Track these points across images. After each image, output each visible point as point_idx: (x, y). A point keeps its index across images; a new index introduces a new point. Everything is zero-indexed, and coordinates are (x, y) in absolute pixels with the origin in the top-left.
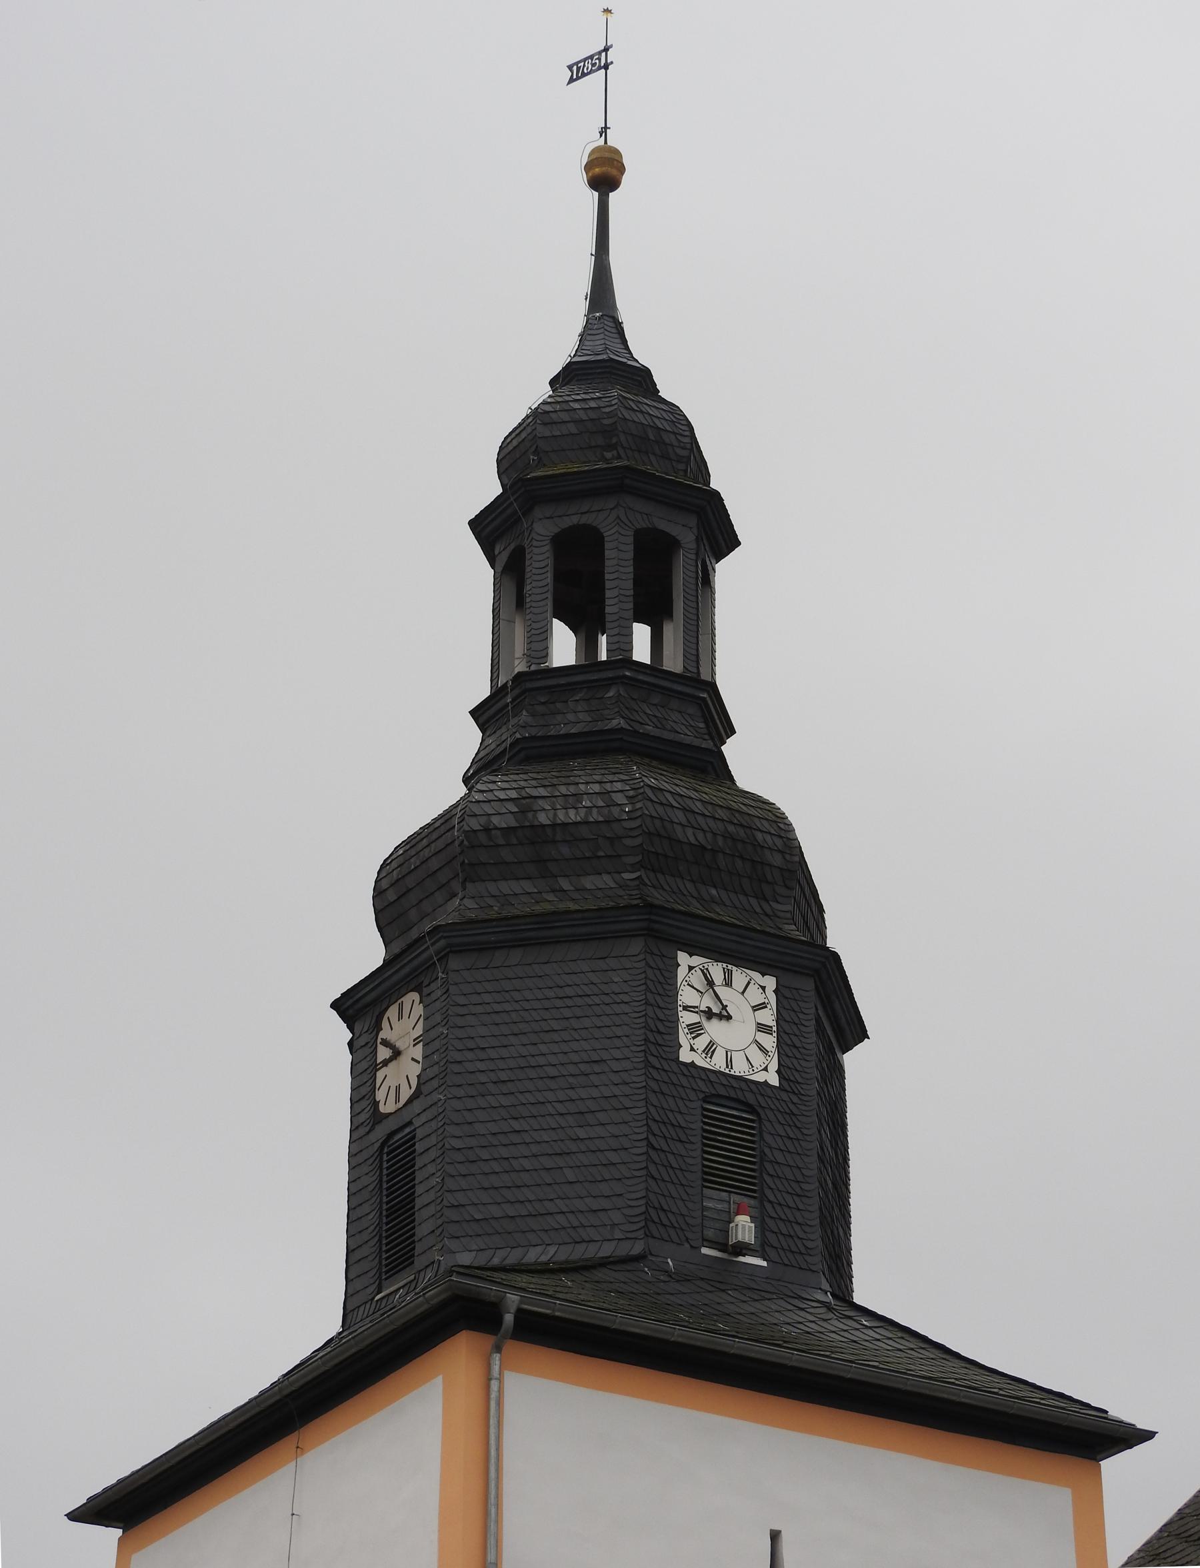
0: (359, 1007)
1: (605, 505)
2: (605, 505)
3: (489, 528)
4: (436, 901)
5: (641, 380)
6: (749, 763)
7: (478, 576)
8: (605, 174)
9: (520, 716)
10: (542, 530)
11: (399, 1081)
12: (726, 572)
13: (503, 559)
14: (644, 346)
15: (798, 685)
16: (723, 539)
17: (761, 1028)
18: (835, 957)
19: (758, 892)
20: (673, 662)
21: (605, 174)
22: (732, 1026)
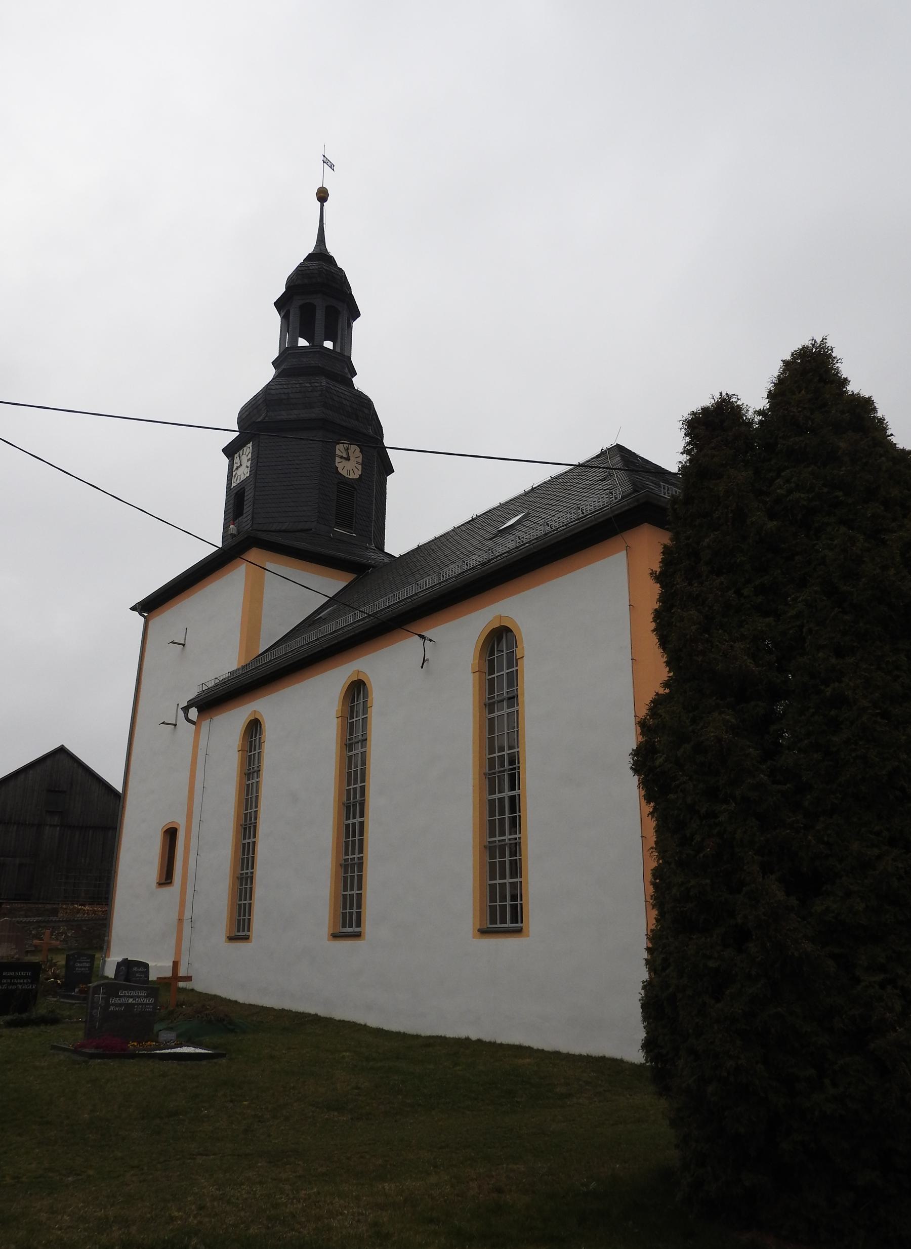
0: (230, 451)
1: (318, 298)
2: (318, 298)
3: (280, 304)
4: (260, 424)
5: (331, 260)
6: (359, 383)
7: (275, 319)
8: (322, 195)
9: (287, 362)
10: (298, 302)
11: (243, 472)
12: (356, 324)
13: (282, 314)
14: (332, 248)
15: (376, 361)
16: (356, 314)
17: (357, 463)
18: (865, 405)
19: (359, 423)
20: (338, 350)
21: (322, 195)
22: (350, 465)
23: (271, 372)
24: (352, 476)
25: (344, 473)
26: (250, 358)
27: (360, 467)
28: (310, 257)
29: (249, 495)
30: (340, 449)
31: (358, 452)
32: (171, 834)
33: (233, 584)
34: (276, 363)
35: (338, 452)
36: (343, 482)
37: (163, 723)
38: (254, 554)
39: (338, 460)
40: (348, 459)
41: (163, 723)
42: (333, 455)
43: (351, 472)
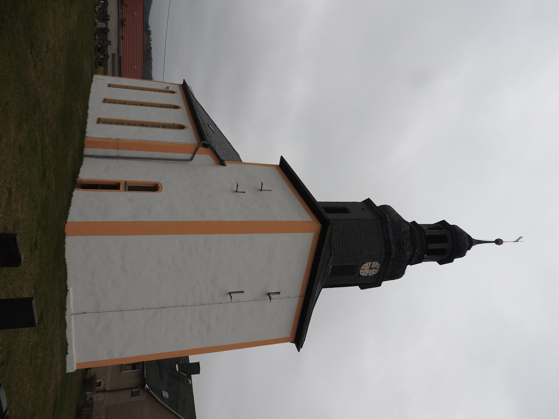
1: (446, 243)
2: (446, 243)
8: (498, 242)
15: (422, 274)
21: (498, 242)
23: (409, 220)
24: (361, 271)
25: (363, 267)
26: (419, 209)
27: (366, 275)
28: (469, 237)
29: (344, 216)
30: (376, 264)
31: (373, 273)
32: (243, 292)
33: (303, 215)
34: (414, 223)
35: (374, 263)
36: (357, 268)
37: (238, 185)
38: (317, 226)
39: (370, 263)
40: (370, 268)
41: (238, 185)
42: (372, 261)
43: (363, 271)
